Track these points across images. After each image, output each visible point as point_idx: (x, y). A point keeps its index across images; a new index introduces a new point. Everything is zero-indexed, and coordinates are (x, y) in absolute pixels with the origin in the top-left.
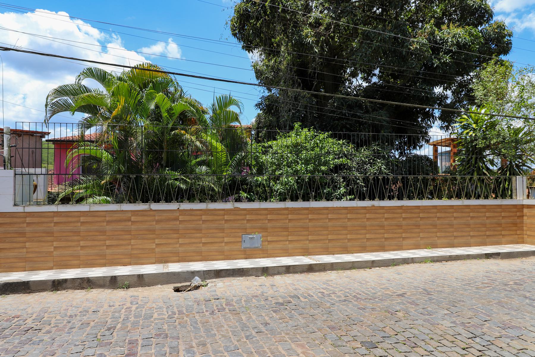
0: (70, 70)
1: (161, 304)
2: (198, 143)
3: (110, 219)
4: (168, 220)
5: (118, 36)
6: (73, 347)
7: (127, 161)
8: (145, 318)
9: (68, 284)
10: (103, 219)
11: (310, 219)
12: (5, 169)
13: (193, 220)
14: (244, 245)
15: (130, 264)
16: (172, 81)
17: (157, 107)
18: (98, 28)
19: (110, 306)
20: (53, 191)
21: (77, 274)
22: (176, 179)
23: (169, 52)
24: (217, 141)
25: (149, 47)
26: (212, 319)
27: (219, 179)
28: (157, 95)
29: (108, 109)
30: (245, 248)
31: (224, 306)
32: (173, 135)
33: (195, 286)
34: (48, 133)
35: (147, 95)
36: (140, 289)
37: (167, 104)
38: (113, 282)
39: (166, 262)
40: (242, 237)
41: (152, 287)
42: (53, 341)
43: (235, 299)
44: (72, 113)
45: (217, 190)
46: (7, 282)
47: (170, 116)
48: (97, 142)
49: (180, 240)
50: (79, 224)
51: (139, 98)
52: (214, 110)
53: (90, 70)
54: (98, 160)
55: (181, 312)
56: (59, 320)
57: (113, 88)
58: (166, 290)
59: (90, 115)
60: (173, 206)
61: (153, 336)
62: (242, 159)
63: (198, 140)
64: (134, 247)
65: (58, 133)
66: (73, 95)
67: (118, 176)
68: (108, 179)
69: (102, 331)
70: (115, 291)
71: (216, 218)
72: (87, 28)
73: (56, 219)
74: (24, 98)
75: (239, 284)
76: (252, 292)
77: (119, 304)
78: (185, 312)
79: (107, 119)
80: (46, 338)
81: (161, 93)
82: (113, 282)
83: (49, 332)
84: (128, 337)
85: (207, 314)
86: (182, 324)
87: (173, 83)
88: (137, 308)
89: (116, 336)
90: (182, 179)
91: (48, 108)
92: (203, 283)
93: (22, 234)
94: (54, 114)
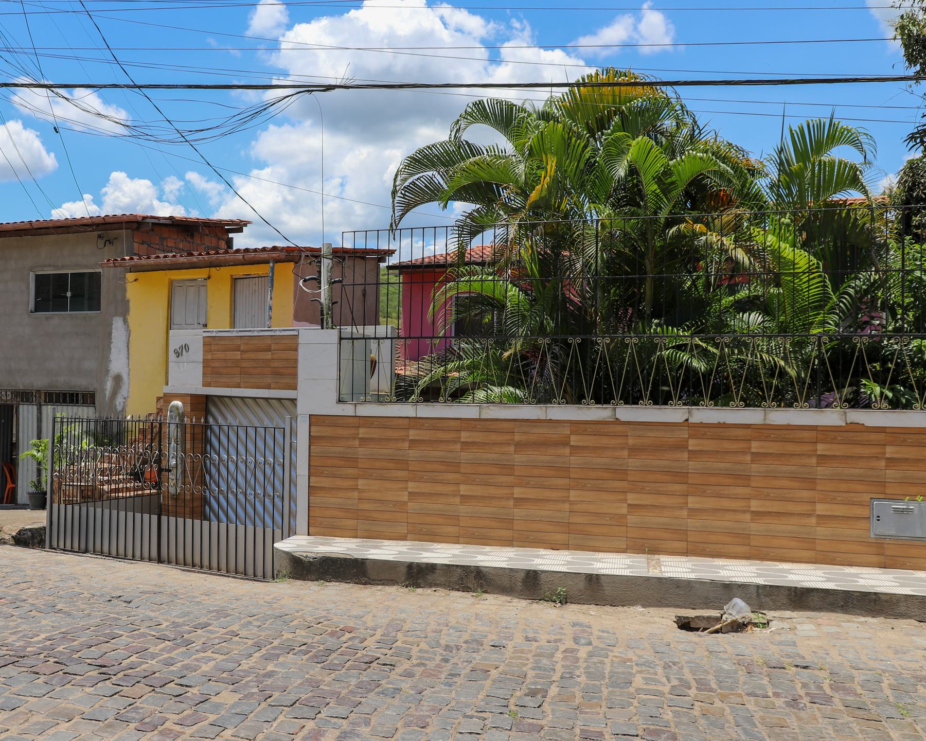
0: (427, 115)
1: (649, 655)
2: (740, 255)
3: (523, 438)
4: (659, 448)
5: (525, 22)
6: (462, 720)
7: (558, 305)
8: (614, 685)
9: (438, 577)
10: (508, 437)
11: (362, 440)
12: (322, 328)
13: (727, 452)
14: (877, 529)
15: (566, 546)
16: (669, 103)
17: (633, 171)
18: (482, 16)
19: (527, 639)
20: (408, 373)
21: (454, 556)
22: (679, 348)
23: (642, 37)
24: (794, 245)
25: (594, 33)
26: (794, 719)
27: (799, 345)
28: (634, 143)
29: (520, 188)
30: (880, 537)
31: (828, 691)
32: (672, 238)
33: (733, 622)
34: (391, 253)
35: (607, 146)
36: (593, 610)
37: (658, 161)
38: (531, 585)
39: (654, 551)
40: (870, 506)
41: (620, 609)
42: (419, 697)
43: (859, 677)
44: (442, 205)
45: (792, 373)
46: (328, 555)
47: (663, 191)
48: (492, 264)
49: (690, 499)
50: (458, 446)
51: (587, 156)
52: (782, 165)
53: (479, 105)
54: (497, 305)
55: (702, 685)
56: (426, 652)
57: (531, 139)
58: (660, 622)
59: (478, 206)
60: (674, 413)
61: (640, 733)
62: (866, 292)
63: (740, 246)
64: (576, 507)
65: (410, 250)
66: (445, 166)
67: (541, 341)
68: (518, 347)
69: (518, 693)
70: (535, 606)
71: (790, 448)
72: (462, 17)
73: (413, 434)
74: (342, 185)
75: (868, 635)
76: (915, 666)
77: (548, 637)
78: (714, 686)
79: (514, 211)
80: (406, 685)
81: (640, 137)
82: (531, 585)
83: (409, 674)
84: (579, 723)
85: (779, 702)
86: (712, 718)
87: (673, 109)
88: (591, 655)
89: (549, 712)
90: (697, 346)
91: (397, 198)
92: (755, 618)
93: (352, 461)
94: (408, 211)
